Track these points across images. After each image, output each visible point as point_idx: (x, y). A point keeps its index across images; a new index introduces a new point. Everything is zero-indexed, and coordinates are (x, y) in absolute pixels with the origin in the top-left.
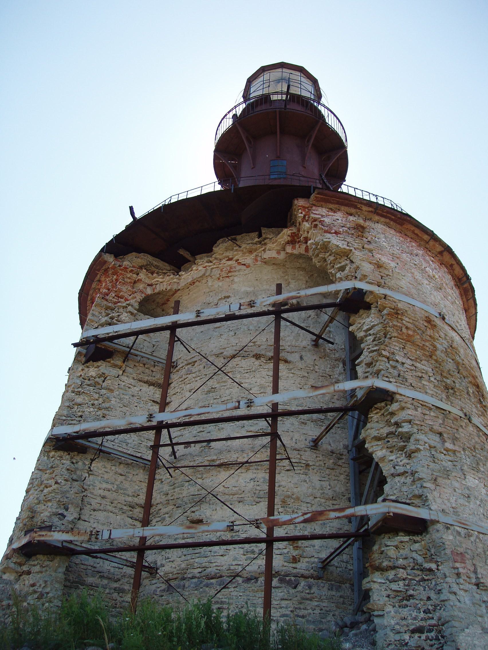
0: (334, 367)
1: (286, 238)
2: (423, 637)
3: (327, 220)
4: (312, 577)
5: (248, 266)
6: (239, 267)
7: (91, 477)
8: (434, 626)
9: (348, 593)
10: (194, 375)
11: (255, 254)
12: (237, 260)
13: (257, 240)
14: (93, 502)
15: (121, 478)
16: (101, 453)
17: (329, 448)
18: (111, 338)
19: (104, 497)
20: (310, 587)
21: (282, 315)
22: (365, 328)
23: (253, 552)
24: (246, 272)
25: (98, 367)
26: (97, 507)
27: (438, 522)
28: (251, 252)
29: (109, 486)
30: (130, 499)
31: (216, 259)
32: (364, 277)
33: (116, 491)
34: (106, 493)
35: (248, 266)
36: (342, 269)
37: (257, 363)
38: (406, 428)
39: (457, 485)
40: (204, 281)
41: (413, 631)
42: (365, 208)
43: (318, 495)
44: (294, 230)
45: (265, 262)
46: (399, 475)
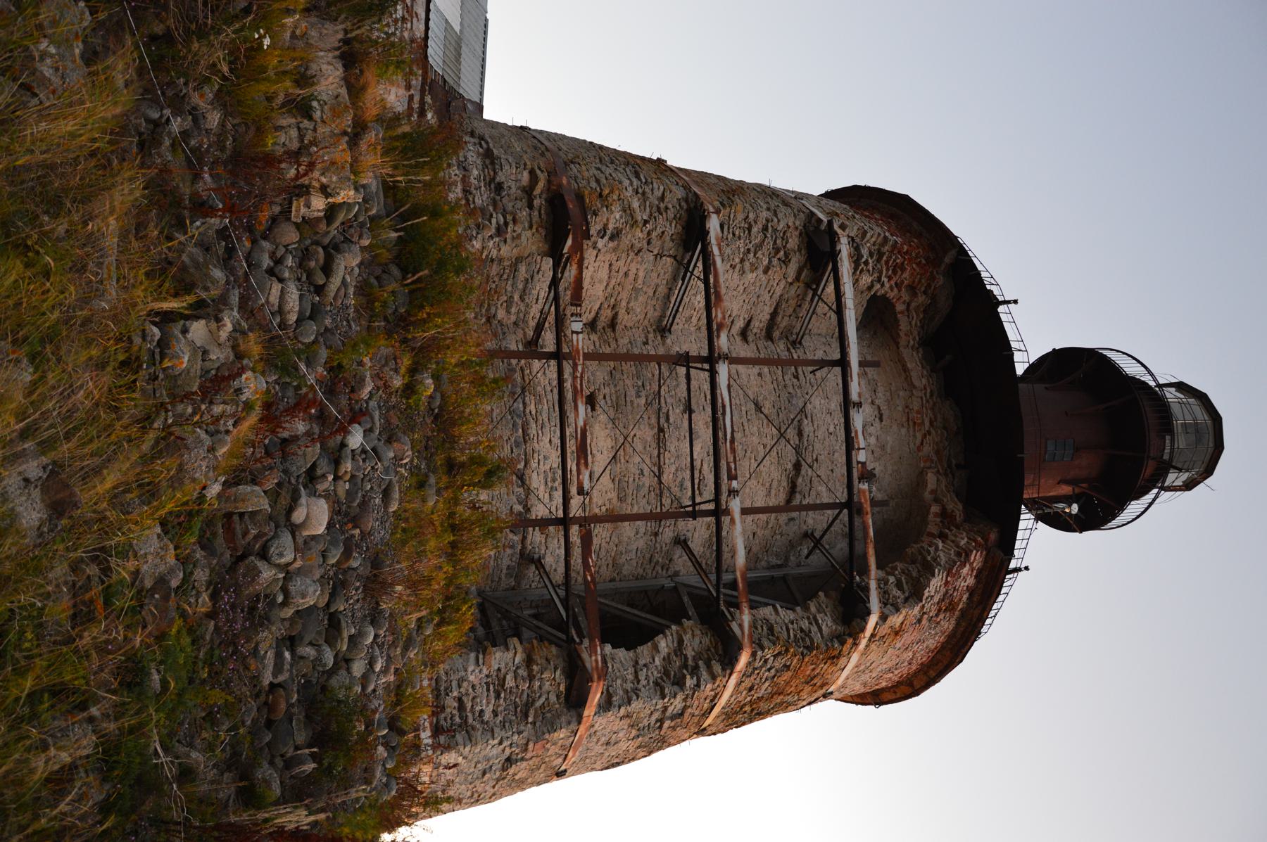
0: (777, 555)
1: (950, 507)
2: (455, 712)
3: (965, 570)
4: (524, 547)
5: (919, 449)
6: (919, 436)
7: (652, 258)
8: (466, 721)
9: (503, 585)
10: (780, 378)
11: (935, 458)
12: (929, 432)
13: (954, 462)
14: (621, 263)
15: (651, 293)
16: (682, 270)
17: (676, 557)
18: (836, 271)
19: (626, 274)
20: (512, 547)
21: (845, 511)
22: (819, 617)
23: (554, 480)
24: (912, 445)
25: (800, 250)
26: (615, 268)
27: (579, 723)
28: (937, 452)
29: (640, 281)
30: (624, 304)
31: (934, 404)
32: (884, 618)
33: (634, 289)
34: (631, 277)
35: (919, 449)
36: (899, 585)
37: (790, 466)
38: (690, 682)
39: (621, 735)
40: (905, 385)
41: (460, 700)
42: (977, 612)
43: (620, 548)
44: (959, 517)
45: (922, 473)
46: (636, 672)
